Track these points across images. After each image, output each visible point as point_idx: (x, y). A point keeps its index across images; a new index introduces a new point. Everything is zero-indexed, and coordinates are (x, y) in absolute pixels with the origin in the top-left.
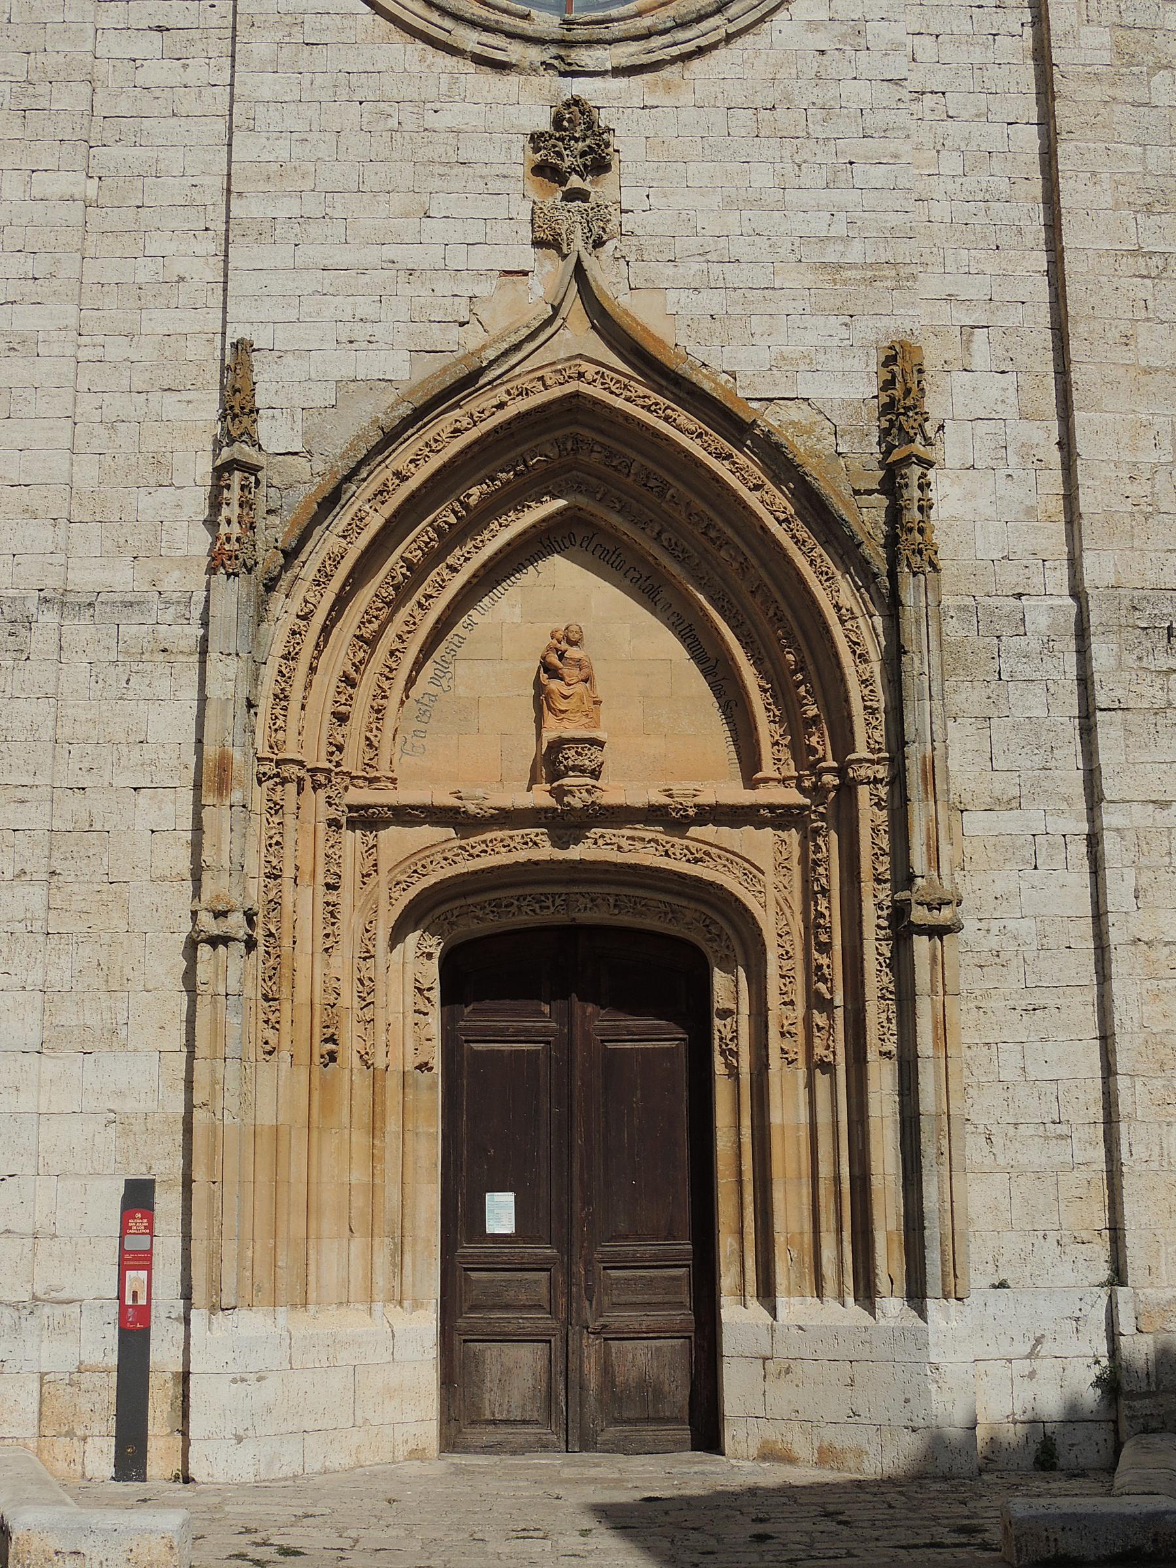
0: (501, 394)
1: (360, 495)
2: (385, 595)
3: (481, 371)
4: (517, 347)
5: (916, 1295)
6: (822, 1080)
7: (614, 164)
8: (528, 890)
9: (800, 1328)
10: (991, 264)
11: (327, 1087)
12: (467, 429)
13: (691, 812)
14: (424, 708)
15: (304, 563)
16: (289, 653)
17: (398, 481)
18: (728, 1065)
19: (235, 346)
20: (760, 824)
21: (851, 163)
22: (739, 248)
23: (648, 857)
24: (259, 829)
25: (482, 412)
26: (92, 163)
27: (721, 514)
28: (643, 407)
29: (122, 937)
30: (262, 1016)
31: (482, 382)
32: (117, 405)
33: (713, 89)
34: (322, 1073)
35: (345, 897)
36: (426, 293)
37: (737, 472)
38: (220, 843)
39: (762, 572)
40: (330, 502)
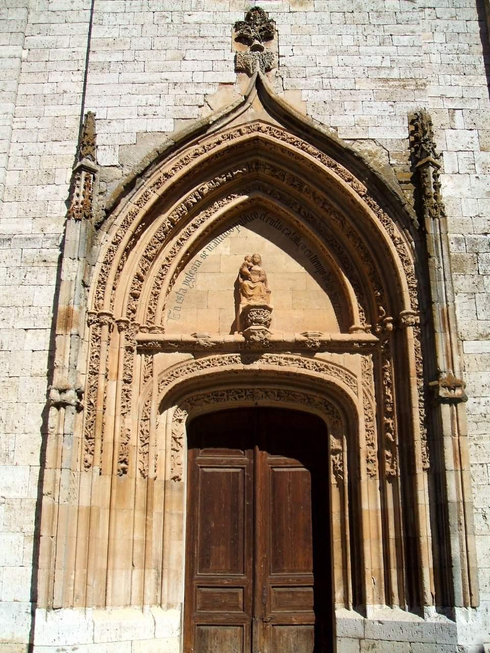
0: (219, 137)
1: (147, 184)
2: (159, 236)
3: (208, 126)
4: (227, 115)
5: (446, 604)
6: (389, 487)
7: (275, 36)
8: (231, 387)
9: (380, 622)
10: (462, 81)
11: (122, 487)
12: (201, 154)
13: (318, 344)
14: (180, 296)
15: (117, 217)
16: (107, 261)
17: (165, 179)
18: (337, 479)
19: (86, 116)
20: (352, 352)
21: (391, 35)
22: (337, 72)
23: (294, 368)
24: (86, 350)
25: (210, 146)
26: (26, 43)
27: (331, 197)
28: (291, 143)
29: (15, 405)
30: (84, 447)
31: (209, 131)
32: (29, 148)
33: (323, 4)
34: (118, 480)
35: (134, 388)
36: (183, 93)
37: (338, 174)
38: (64, 354)
39: (352, 224)
40: (130, 186)
